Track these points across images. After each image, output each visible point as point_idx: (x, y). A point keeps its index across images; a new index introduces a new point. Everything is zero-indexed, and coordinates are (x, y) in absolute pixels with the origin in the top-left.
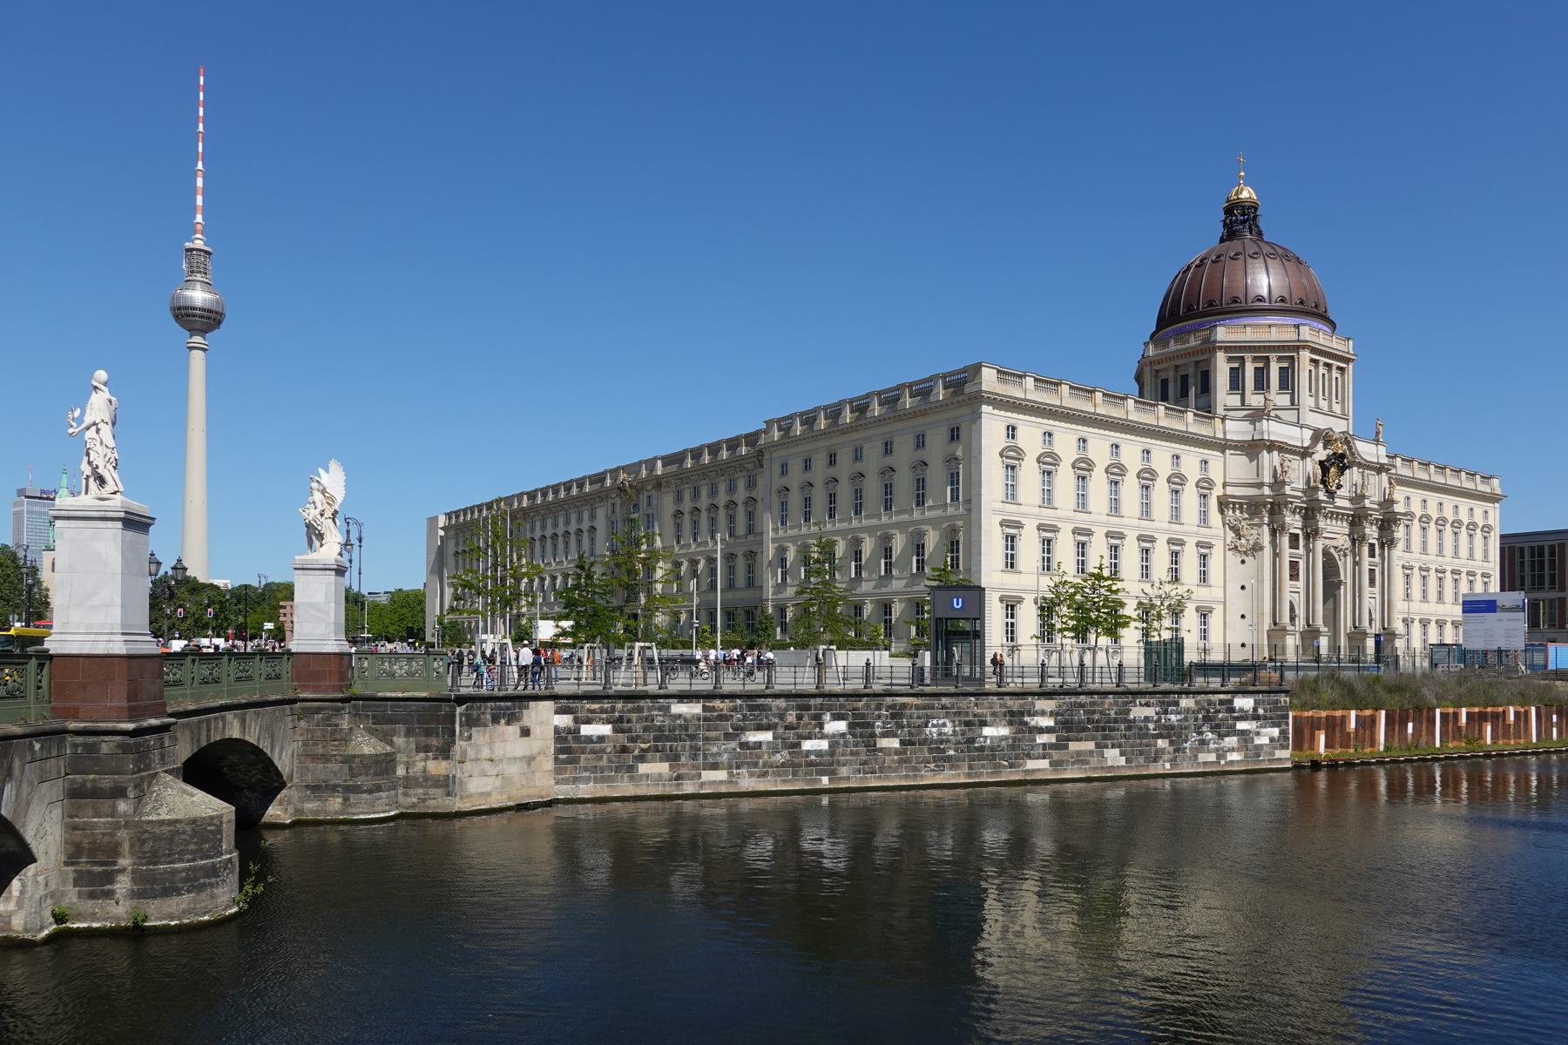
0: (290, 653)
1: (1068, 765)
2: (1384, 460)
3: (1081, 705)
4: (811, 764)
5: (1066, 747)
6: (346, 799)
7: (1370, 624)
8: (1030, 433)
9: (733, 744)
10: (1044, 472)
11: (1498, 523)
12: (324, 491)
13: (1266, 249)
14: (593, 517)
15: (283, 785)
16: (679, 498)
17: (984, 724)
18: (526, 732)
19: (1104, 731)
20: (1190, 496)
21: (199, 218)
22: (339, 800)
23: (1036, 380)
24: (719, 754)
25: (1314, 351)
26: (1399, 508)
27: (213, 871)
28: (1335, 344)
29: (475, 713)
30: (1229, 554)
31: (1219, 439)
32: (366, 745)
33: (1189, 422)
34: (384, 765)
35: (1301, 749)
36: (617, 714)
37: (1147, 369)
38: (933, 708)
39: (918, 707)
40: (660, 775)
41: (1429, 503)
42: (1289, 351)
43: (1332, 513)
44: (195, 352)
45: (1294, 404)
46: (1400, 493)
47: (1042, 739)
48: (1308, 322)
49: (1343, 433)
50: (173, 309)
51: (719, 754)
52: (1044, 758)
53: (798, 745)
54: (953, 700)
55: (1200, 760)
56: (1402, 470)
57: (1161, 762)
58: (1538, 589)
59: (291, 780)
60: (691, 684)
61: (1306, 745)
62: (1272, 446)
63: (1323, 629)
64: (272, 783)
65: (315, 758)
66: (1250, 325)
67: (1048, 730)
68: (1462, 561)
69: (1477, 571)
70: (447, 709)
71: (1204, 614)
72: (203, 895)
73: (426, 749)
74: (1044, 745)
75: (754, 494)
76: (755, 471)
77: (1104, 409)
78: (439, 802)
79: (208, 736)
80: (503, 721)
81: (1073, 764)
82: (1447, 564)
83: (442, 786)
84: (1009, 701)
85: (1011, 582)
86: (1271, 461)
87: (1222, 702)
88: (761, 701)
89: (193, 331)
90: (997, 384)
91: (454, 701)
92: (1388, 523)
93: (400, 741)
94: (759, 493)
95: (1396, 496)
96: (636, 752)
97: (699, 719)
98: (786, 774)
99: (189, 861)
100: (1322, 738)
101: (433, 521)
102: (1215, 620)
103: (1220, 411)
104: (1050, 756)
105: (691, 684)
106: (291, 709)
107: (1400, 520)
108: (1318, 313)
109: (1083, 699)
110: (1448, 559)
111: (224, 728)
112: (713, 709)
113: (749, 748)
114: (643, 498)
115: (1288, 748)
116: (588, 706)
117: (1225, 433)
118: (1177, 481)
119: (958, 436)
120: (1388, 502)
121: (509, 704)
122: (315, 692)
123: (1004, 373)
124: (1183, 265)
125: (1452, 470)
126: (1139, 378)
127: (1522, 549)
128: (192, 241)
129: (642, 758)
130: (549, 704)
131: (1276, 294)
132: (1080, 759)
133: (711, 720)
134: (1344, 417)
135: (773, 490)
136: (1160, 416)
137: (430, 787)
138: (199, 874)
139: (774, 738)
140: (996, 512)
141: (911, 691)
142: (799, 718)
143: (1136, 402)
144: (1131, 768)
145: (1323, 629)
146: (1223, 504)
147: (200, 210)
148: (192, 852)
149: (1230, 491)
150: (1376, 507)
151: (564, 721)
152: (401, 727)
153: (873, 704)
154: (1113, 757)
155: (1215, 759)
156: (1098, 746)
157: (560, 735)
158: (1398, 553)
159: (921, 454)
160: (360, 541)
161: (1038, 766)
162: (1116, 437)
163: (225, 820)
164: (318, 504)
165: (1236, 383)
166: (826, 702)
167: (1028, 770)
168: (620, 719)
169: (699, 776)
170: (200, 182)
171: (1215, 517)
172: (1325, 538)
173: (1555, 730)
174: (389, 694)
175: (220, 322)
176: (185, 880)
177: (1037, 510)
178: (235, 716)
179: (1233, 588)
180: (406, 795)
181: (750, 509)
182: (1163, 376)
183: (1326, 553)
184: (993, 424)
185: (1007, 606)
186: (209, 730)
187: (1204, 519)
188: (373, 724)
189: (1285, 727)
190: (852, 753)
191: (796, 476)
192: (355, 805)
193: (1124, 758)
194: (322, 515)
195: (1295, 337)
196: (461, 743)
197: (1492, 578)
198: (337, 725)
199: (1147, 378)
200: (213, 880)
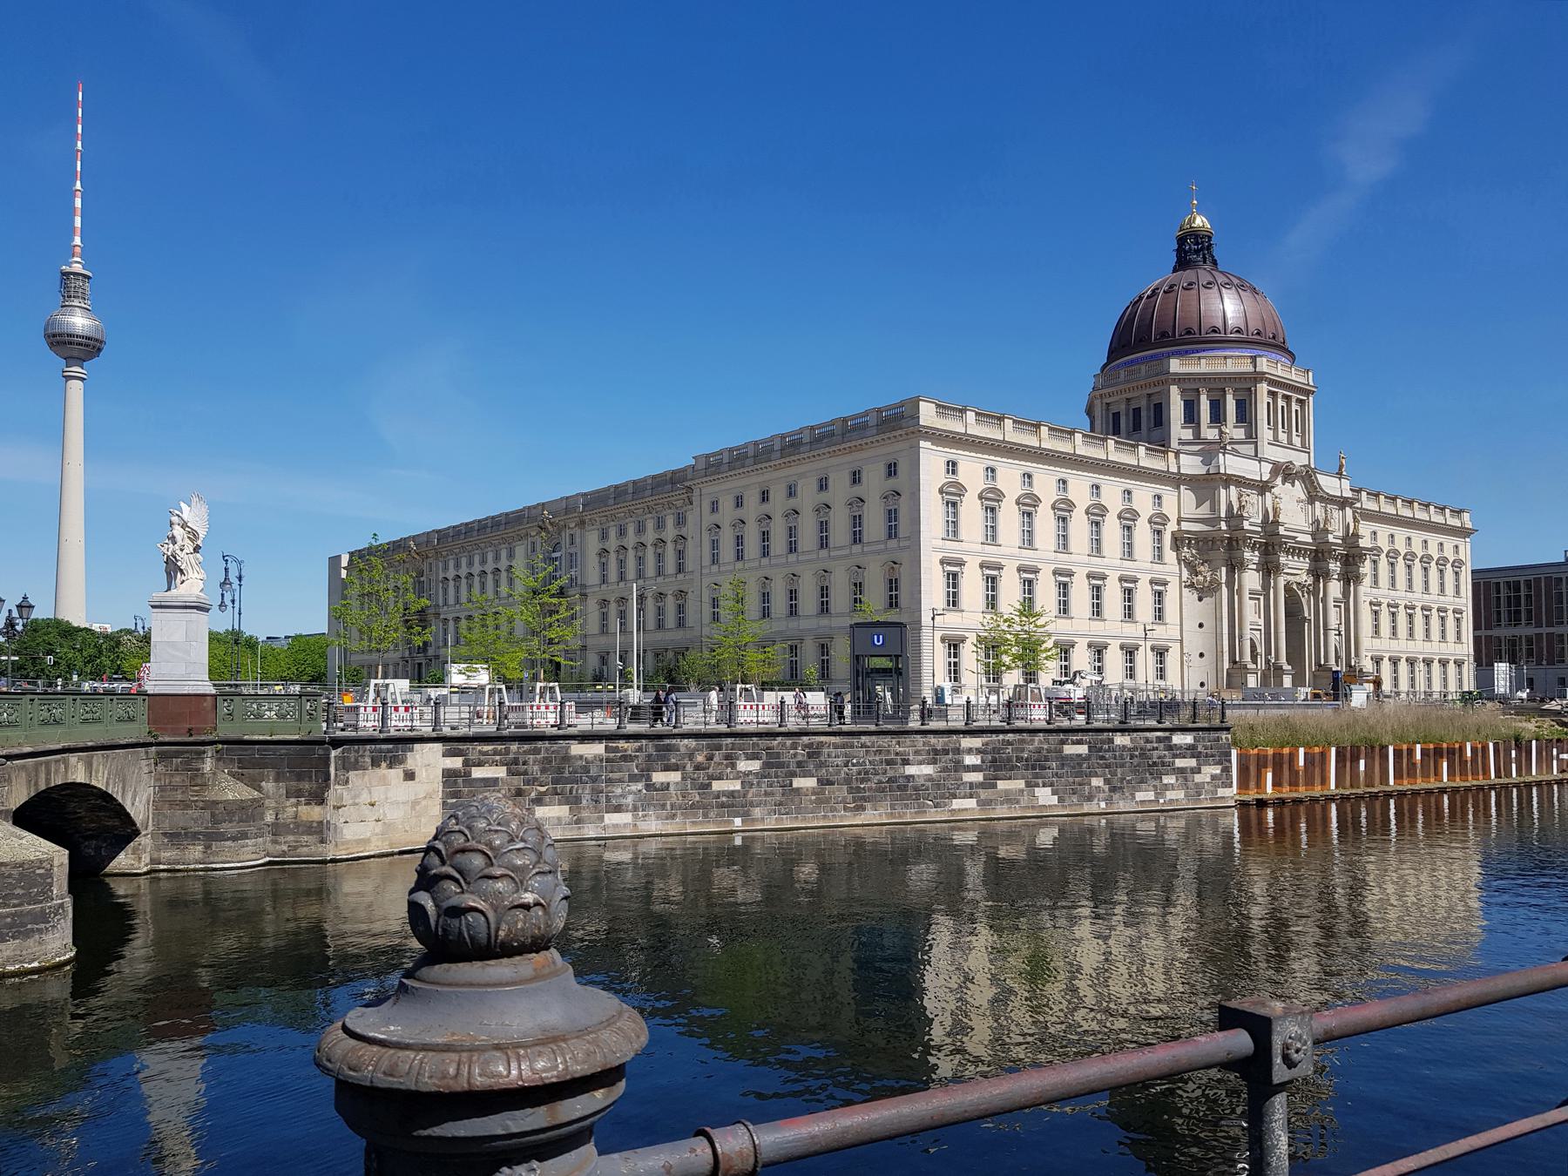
0: (145, 694)
1: (996, 804)
2: (1348, 494)
3: (1009, 743)
4: (723, 805)
5: (995, 786)
6: (208, 847)
7: (1337, 662)
8: (972, 469)
9: (640, 786)
10: (1024, 513)
11: (1469, 557)
12: (184, 525)
13: (1221, 279)
14: (511, 556)
15: (137, 833)
16: (604, 536)
17: (906, 762)
18: (410, 776)
19: (1036, 769)
20: (1143, 533)
21: (78, 240)
22: (200, 848)
23: (977, 414)
24: (623, 796)
25: (1272, 382)
26: (1365, 542)
27: (43, 917)
28: (1295, 376)
30: (1185, 591)
31: (1173, 473)
32: (233, 791)
33: (1143, 457)
35: (1247, 788)
36: (511, 756)
37: (1097, 402)
38: (852, 747)
39: (836, 746)
40: (559, 819)
41: (1446, 546)
42: (1246, 385)
43: (1294, 548)
44: (73, 383)
45: (1252, 437)
46: (1365, 529)
47: (971, 777)
48: (1263, 353)
49: (1304, 466)
50: (47, 336)
52: (971, 797)
53: (709, 785)
54: (874, 738)
55: (1137, 799)
56: (1368, 504)
57: (1096, 801)
58: (1515, 625)
59: (146, 829)
60: (592, 724)
61: (1252, 784)
62: (1229, 480)
63: (1287, 667)
64: (123, 831)
65: (172, 804)
66: (1204, 357)
67: (975, 768)
68: (1416, 595)
69: (1448, 607)
70: (321, 752)
71: (1161, 653)
72: (30, 942)
73: (298, 794)
74: (971, 783)
75: (684, 532)
76: (685, 508)
77: (1049, 443)
78: (310, 849)
79: (48, 780)
80: (384, 765)
81: (1002, 803)
82: (1400, 598)
83: (316, 833)
84: (933, 740)
85: (952, 621)
86: (1228, 496)
87: (1159, 740)
88: (667, 741)
89: (70, 360)
90: (938, 419)
91: (328, 744)
92: (1352, 557)
93: (269, 786)
94: (690, 529)
95: (1361, 532)
96: (533, 795)
97: (601, 760)
98: (695, 815)
99: (14, 906)
100: (1269, 776)
101: (334, 561)
102: (1172, 659)
103: (1174, 444)
104: (978, 796)
105: (592, 724)
106: (147, 753)
107: (1365, 555)
108: (1277, 345)
109: (1010, 737)
110: (1418, 595)
111: (66, 771)
112: (616, 750)
113: (656, 790)
114: (566, 535)
115: (1231, 787)
116: (479, 748)
117: (1179, 468)
118: (1128, 519)
119: (895, 471)
120: (1351, 539)
121: (391, 746)
122: (175, 735)
123: (944, 407)
124: (1134, 296)
125: (1420, 504)
126: (1090, 412)
127: (1498, 584)
128: (69, 265)
129: (539, 801)
130: (438, 747)
131: (1251, 329)
132: (1009, 798)
133: (614, 761)
134: (1304, 448)
135: (704, 528)
136: (1112, 451)
137: (303, 834)
138: (25, 920)
139: (683, 778)
140: (936, 549)
141: (830, 730)
142: (710, 758)
143: (1084, 436)
145: (1287, 667)
146: (1178, 541)
147: (78, 232)
148: (18, 896)
149: (1185, 526)
150: (1340, 541)
151: (456, 763)
152: (271, 773)
153: (789, 742)
154: (1045, 796)
155: (1153, 798)
156: (1028, 785)
157: (449, 775)
158: (1365, 587)
159: (858, 490)
160: (240, 580)
161: (965, 805)
162: (1063, 472)
163: (56, 863)
164: (179, 538)
165: (1191, 416)
166: (738, 741)
167: (954, 810)
168: (516, 762)
169: (602, 819)
170: (78, 203)
171: (1170, 555)
172: (1288, 574)
173: (1514, 766)
174: (256, 738)
175: (99, 350)
176: (10, 926)
177: (941, 543)
178: (80, 759)
179: (1190, 625)
180: (275, 842)
181: (680, 547)
182: (1114, 409)
183: (1288, 588)
184: (932, 462)
185: (950, 645)
186: (48, 773)
187: (1159, 556)
188: (239, 768)
189: (1228, 764)
190: (766, 794)
191: (727, 512)
193: (1056, 797)
194: (182, 550)
195: (1251, 369)
196: (337, 787)
197: (1465, 613)
198: (198, 770)
199: (1098, 412)
200: (43, 926)
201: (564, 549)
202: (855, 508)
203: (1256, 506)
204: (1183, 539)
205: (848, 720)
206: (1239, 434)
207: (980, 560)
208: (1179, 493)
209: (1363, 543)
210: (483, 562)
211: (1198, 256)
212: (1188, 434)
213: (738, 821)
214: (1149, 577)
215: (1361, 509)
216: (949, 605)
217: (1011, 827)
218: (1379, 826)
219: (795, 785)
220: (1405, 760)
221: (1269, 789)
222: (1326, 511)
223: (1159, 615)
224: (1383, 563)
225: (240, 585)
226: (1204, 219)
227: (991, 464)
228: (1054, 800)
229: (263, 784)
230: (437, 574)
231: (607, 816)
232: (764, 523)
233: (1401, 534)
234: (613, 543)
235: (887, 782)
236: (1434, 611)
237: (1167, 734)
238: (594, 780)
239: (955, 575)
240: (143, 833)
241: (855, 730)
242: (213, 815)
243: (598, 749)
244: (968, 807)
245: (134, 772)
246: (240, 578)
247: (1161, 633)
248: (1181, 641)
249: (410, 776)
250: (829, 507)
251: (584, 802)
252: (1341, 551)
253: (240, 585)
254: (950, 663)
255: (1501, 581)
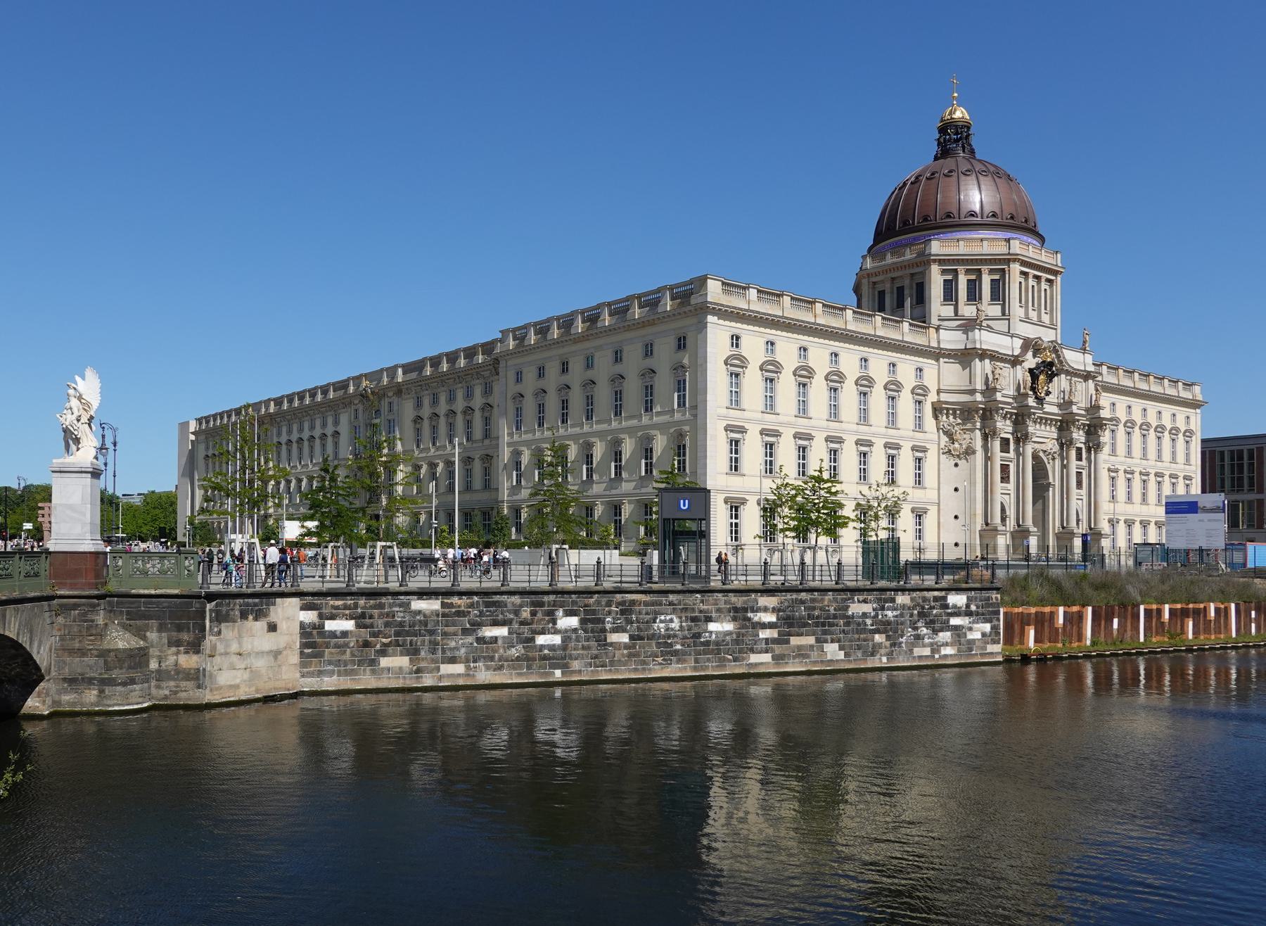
0: (47, 552)
2: (1091, 368)
3: (802, 602)
4: (544, 658)
5: (788, 642)
6: (101, 691)
7: (1078, 524)
8: (754, 342)
9: (470, 639)
11: (1199, 428)
12: (80, 398)
13: (978, 167)
14: (336, 423)
15: (41, 678)
16: (419, 405)
18: (272, 628)
19: (824, 626)
22: (95, 692)
23: (759, 291)
24: (457, 648)
25: (1024, 263)
29: (224, 609)
30: (943, 457)
31: (933, 348)
32: (120, 640)
33: (905, 332)
34: (137, 658)
36: (359, 610)
37: (865, 281)
38: (661, 604)
40: (401, 668)
41: (1149, 411)
42: (1000, 264)
43: (1041, 418)
46: (1105, 400)
47: (764, 634)
48: (1019, 236)
49: (1052, 342)
51: (457, 648)
52: (767, 652)
53: (533, 640)
54: (680, 597)
55: (915, 655)
56: (1108, 377)
57: (878, 656)
58: (1238, 491)
61: (1016, 640)
62: (984, 355)
65: (71, 652)
67: (771, 626)
70: (198, 605)
71: (919, 515)
73: (178, 643)
74: (767, 639)
75: (490, 401)
76: (491, 378)
77: (823, 318)
80: (251, 617)
81: (794, 657)
84: (733, 598)
85: (735, 484)
86: (983, 369)
87: (936, 599)
88: (497, 598)
91: (205, 598)
92: (1094, 427)
93: (152, 636)
94: (495, 399)
96: (378, 647)
97: (438, 615)
98: (521, 667)
100: (1032, 633)
101: (184, 426)
102: (930, 521)
103: (935, 321)
104: (772, 651)
106: (49, 605)
107: (1105, 425)
108: (1028, 228)
109: (803, 595)
110: (1152, 463)
112: (451, 605)
113: (485, 643)
115: (999, 643)
116: (332, 602)
117: (939, 342)
119: (684, 344)
120: (1094, 408)
121: (257, 600)
122: (71, 589)
123: (728, 285)
125: (1170, 381)
126: (857, 290)
127: (1222, 453)
129: (383, 653)
130: (295, 601)
132: (801, 653)
133: (450, 615)
134: (1052, 326)
136: (877, 326)
137: (182, 680)
139: (510, 633)
140: (721, 417)
142: (533, 614)
144: (850, 661)
146: (937, 410)
149: (944, 397)
150: (1083, 412)
151: (310, 617)
153: (604, 600)
154: (833, 651)
155: (929, 654)
156: (818, 640)
157: (305, 630)
158: (1104, 456)
160: (115, 446)
161: (761, 659)
164: (75, 410)
165: (950, 294)
166: (559, 598)
167: (751, 664)
168: (363, 616)
171: (930, 422)
172: (1035, 442)
173: (1253, 625)
174: (142, 592)
179: (947, 490)
180: (158, 687)
181: (487, 414)
182: (880, 287)
183: (1035, 457)
184: (718, 334)
185: (732, 507)
187: (919, 424)
188: (127, 619)
189: (996, 623)
192: (109, 697)
193: (843, 652)
194: (78, 420)
195: (1005, 250)
196: (212, 638)
197: (1194, 481)
198: (93, 621)
199: (865, 289)
201: (383, 416)
202: (648, 379)
203: (1008, 379)
204: (942, 409)
205: (656, 579)
206: (995, 310)
207: (825, 435)
208: (939, 366)
209: (1105, 414)
210: (324, 425)
211: (958, 145)
212: (948, 311)
213: (558, 673)
214: (911, 444)
215: (1101, 382)
216: (731, 470)
217: (644, 669)
218: (1130, 681)
219: (327, 628)
220: (1154, 620)
221: (1031, 643)
222: (1071, 383)
223: (919, 479)
224: (1121, 431)
225: (115, 450)
226: (963, 110)
227: (771, 338)
228: (841, 655)
229: (148, 634)
230: (272, 440)
231: (442, 666)
232: (563, 392)
233: (1138, 404)
234: (426, 411)
235: (692, 638)
236: (1181, 479)
237: (943, 594)
238: (432, 633)
239: (737, 442)
240: (47, 678)
241: (664, 589)
242: (106, 662)
243: (433, 605)
244: (764, 661)
245: (39, 623)
246: (115, 444)
247: (917, 496)
248: (939, 504)
249: (272, 628)
250: (623, 378)
251: (423, 653)
252: (1084, 421)
253: (115, 450)
254: (732, 524)
255: (1226, 449)
